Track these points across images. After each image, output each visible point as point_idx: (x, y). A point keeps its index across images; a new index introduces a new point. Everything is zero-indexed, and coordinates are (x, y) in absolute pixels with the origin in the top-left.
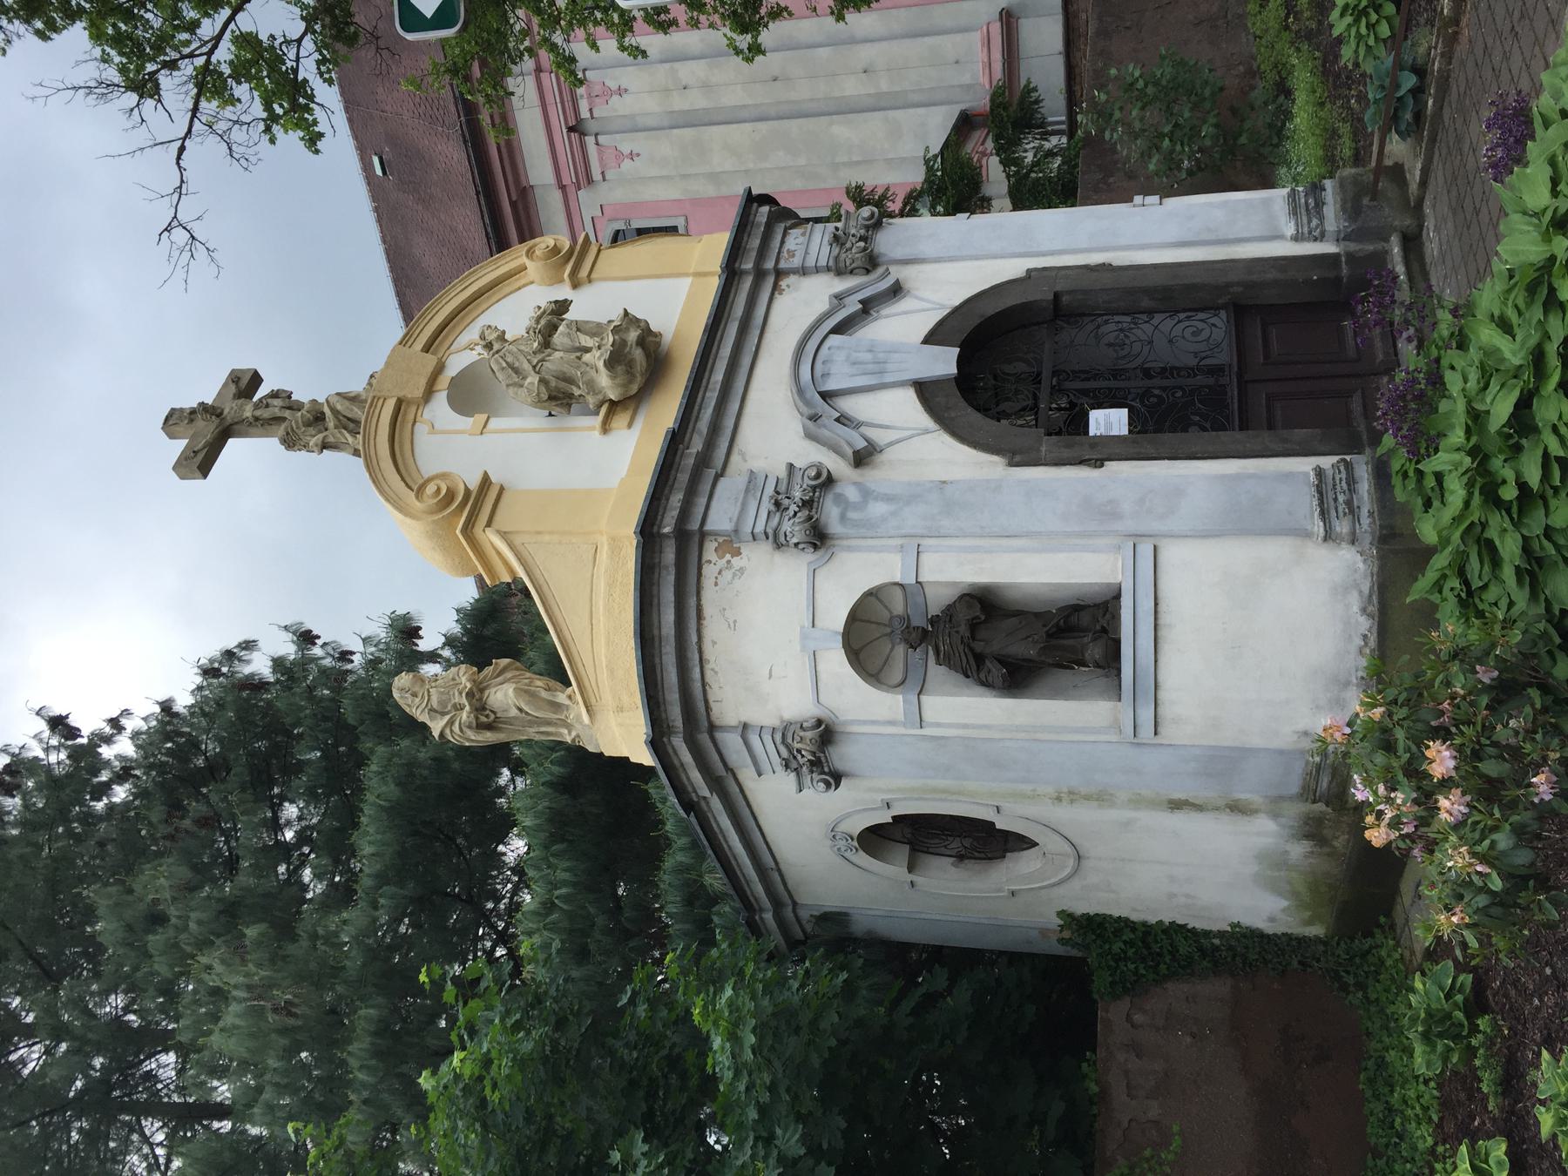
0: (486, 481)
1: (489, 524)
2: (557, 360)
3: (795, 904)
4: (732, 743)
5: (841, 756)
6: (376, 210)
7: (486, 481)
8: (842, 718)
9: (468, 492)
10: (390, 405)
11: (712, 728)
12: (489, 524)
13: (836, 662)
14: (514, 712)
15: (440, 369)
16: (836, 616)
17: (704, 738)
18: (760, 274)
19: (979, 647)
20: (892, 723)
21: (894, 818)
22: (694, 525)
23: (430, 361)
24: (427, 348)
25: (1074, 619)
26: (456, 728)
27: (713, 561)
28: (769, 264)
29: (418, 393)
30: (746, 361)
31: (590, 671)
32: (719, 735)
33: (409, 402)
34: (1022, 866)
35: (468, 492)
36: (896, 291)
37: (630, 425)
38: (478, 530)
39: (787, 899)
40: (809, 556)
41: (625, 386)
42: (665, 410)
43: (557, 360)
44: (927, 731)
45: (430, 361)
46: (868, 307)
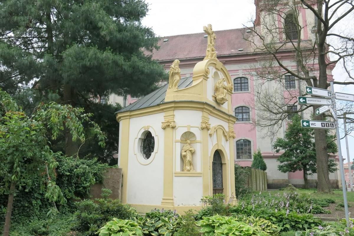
0: (208, 78)
1: (204, 79)
2: (221, 89)
3: (130, 118)
4: (171, 113)
5: (169, 130)
6: (197, 34)
7: (208, 78)
8: (176, 130)
9: (207, 75)
10: (215, 63)
11: (174, 110)
12: (204, 79)
13: (186, 130)
14: (175, 79)
15: (219, 70)
16: (192, 130)
17: (173, 109)
18: (229, 120)
19: (188, 151)
20: (175, 138)
21: (153, 137)
22: (204, 110)
23: (220, 69)
24: (221, 69)
25: (192, 165)
26: (173, 70)
27: (201, 112)
28: (230, 122)
29: (217, 67)
30: (218, 117)
31: (182, 92)
32: (173, 111)
33: (215, 66)
34: (141, 157)
35: (207, 75)
36: (227, 140)
37: (213, 100)
38: (203, 77)
39: (130, 117)
40: (200, 127)
41: (219, 100)
42: (214, 104)
43: (221, 89)
44: (174, 143)
45: (220, 69)
46: (225, 136)
